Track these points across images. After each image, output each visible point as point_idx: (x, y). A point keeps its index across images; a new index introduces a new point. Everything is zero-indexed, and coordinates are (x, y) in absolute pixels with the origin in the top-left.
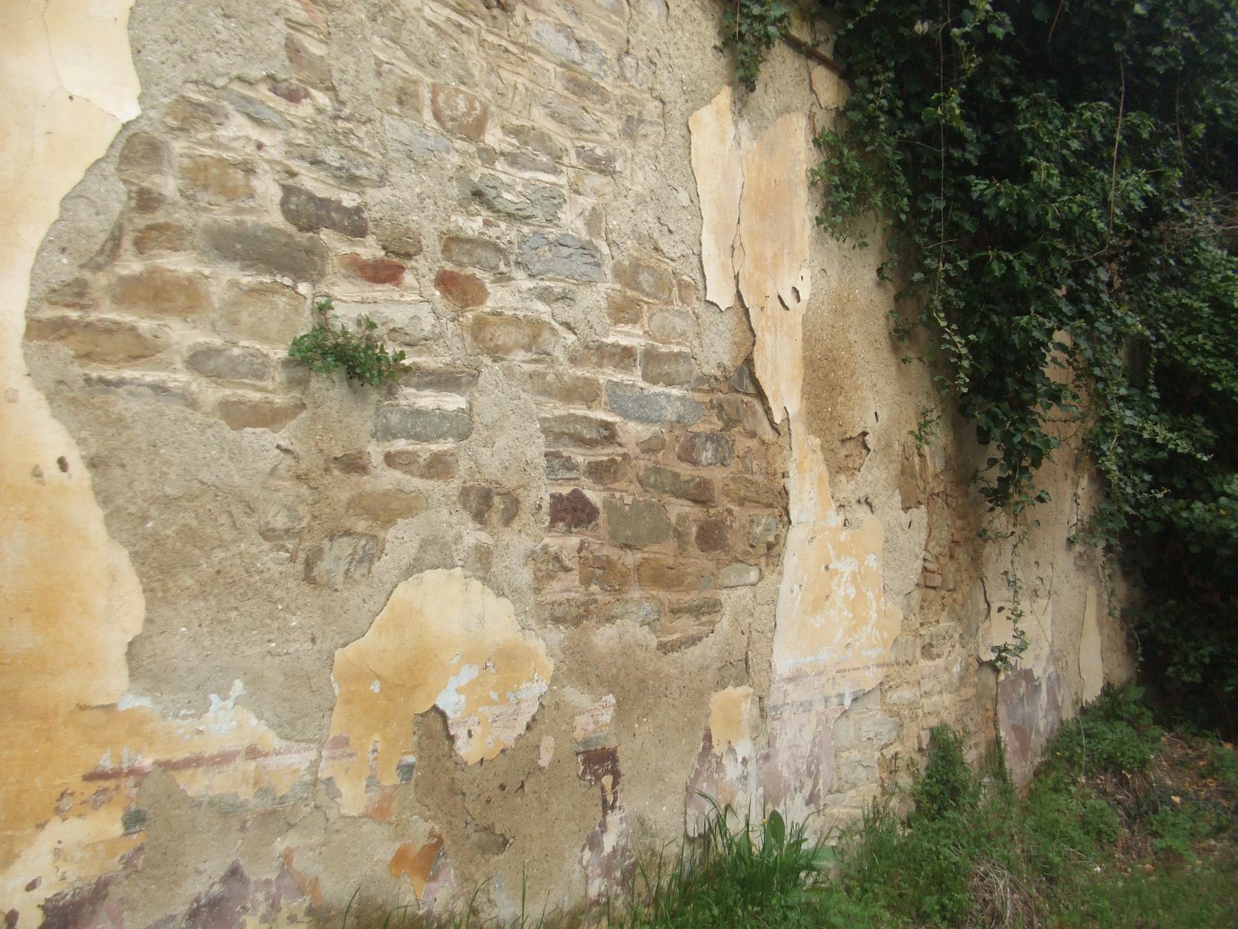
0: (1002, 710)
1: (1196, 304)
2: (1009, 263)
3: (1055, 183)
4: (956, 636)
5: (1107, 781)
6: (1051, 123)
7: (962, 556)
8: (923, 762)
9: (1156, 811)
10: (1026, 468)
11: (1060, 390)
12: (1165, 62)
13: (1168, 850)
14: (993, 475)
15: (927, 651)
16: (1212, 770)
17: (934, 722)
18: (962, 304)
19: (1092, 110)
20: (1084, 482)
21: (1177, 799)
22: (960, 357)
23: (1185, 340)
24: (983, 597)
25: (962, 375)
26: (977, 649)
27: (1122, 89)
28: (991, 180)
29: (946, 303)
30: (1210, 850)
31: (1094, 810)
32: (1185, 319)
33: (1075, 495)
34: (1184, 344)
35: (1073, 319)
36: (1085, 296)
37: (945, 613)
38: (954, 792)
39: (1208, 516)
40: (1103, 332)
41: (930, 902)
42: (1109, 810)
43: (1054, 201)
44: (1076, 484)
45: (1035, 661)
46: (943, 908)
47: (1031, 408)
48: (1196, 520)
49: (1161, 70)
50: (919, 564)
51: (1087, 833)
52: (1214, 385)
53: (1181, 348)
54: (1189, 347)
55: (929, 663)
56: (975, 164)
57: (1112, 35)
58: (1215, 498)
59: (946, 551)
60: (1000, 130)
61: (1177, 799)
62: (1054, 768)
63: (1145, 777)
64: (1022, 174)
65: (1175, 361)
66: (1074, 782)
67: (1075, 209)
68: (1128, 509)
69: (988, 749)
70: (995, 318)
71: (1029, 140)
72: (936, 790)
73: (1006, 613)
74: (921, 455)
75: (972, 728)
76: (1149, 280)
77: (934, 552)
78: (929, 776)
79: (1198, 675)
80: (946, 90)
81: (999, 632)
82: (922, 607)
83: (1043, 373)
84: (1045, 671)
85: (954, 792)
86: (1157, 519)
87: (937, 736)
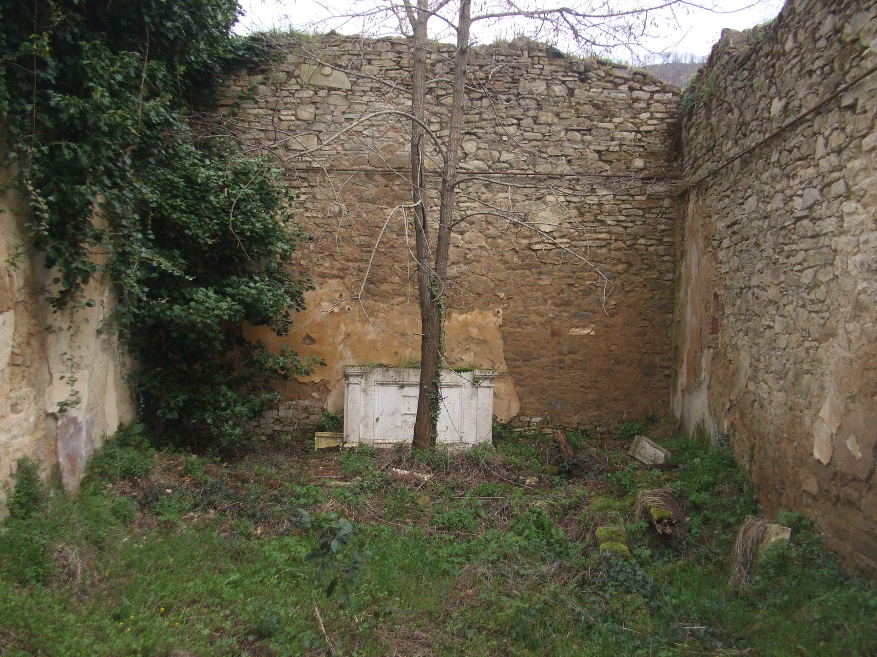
0: (60, 445)
1: (176, 180)
2: (74, 150)
3: (107, 101)
4: (32, 397)
5: (127, 486)
6: (103, 61)
7: (35, 344)
8: (13, 483)
9: (157, 500)
10: (78, 284)
11: (101, 234)
12: (173, 32)
13: (168, 521)
14: (55, 290)
15: (14, 408)
16: (188, 471)
17: (19, 455)
18: (43, 176)
19: (130, 57)
20: (106, 293)
21: (169, 491)
22: (42, 211)
23: (169, 202)
24: (47, 371)
25: (44, 223)
26: (44, 405)
27: (147, 45)
28: (65, 95)
29: (33, 175)
30: (192, 518)
31: (120, 504)
32: (169, 188)
33: (102, 301)
34: (168, 204)
35: (110, 188)
36: (117, 173)
37: (24, 382)
38: (36, 500)
39: (183, 314)
40: (127, 197)
41: (29, 572)
42: (129, 503)
43: (104, 113)
44: (102, 294)
45: (78, 413)
46: (38, 575)
47: (82, 245)
48: (176, 317)
49: (171, 36)
50: (9, 350)
51: (118, 518)
52: (187, 231)
53: (167, 207)
54: (172, 207)
55: (16, 416)
56: (54, 82)
57: (144, 10)
58: (187, 302)
59: (25, 340)
60: (70, 61)
61: (169, 491)
62: (94, 480)
63: (149, 480)
64: (86, 94)
65: (163, 215)
66: (105, 488)
67: (118, 119)
68: (135, 310)
69: (52, 471)
70: (63, 186)
71: (89, 71)
72: (24, 500)
73: (66, 380)
74: (10, 276)
75: (42, 458)
76: (150, 163)
77: (18, 341)
78: (18, 492)
79: (176, 414)
80: (40, 33)
81: (59, 393)
82: (11, 379)
83: (90, 223)
84: (85, 417)
85: (36, 500)
86: (150, 316)
87: (22, 465)
